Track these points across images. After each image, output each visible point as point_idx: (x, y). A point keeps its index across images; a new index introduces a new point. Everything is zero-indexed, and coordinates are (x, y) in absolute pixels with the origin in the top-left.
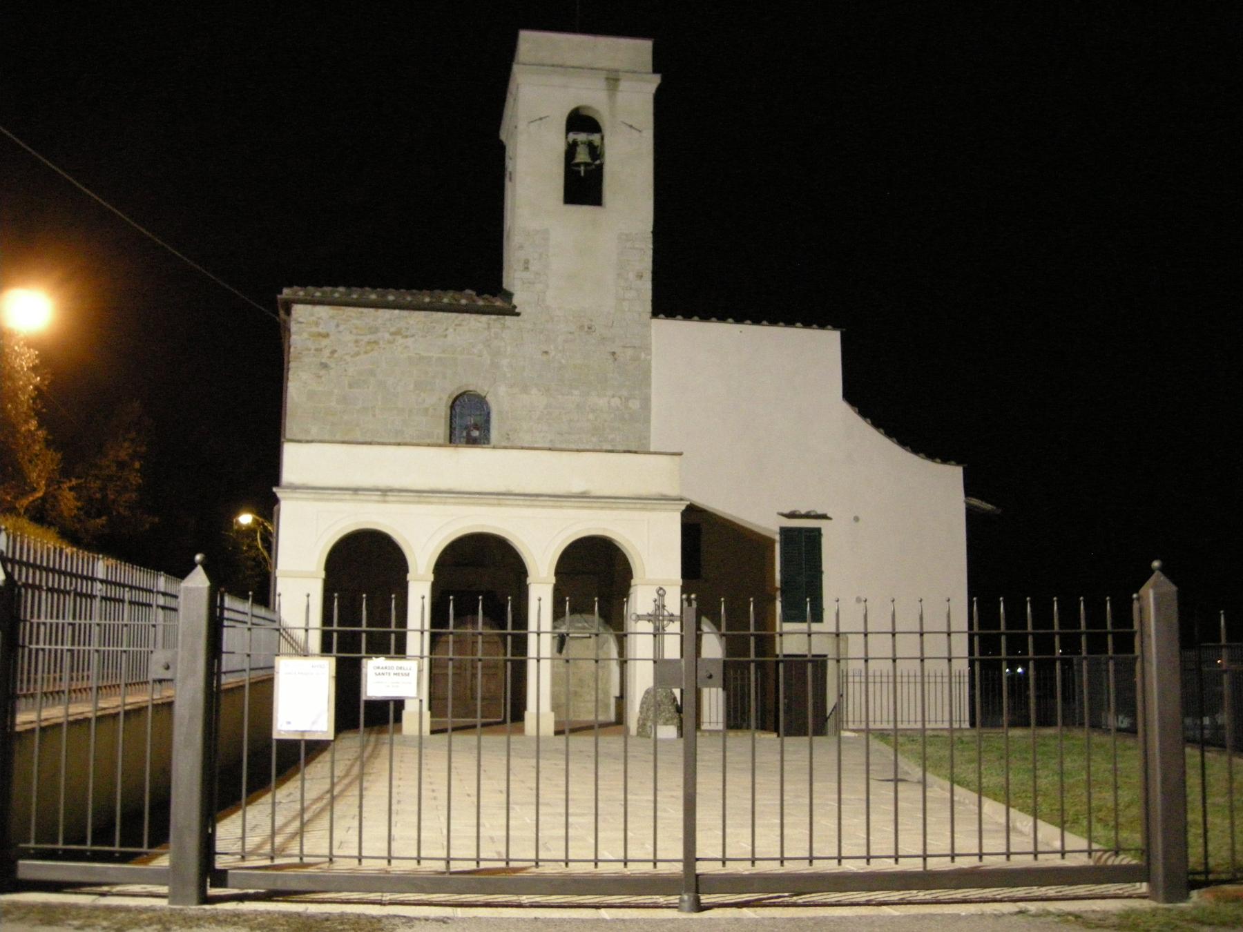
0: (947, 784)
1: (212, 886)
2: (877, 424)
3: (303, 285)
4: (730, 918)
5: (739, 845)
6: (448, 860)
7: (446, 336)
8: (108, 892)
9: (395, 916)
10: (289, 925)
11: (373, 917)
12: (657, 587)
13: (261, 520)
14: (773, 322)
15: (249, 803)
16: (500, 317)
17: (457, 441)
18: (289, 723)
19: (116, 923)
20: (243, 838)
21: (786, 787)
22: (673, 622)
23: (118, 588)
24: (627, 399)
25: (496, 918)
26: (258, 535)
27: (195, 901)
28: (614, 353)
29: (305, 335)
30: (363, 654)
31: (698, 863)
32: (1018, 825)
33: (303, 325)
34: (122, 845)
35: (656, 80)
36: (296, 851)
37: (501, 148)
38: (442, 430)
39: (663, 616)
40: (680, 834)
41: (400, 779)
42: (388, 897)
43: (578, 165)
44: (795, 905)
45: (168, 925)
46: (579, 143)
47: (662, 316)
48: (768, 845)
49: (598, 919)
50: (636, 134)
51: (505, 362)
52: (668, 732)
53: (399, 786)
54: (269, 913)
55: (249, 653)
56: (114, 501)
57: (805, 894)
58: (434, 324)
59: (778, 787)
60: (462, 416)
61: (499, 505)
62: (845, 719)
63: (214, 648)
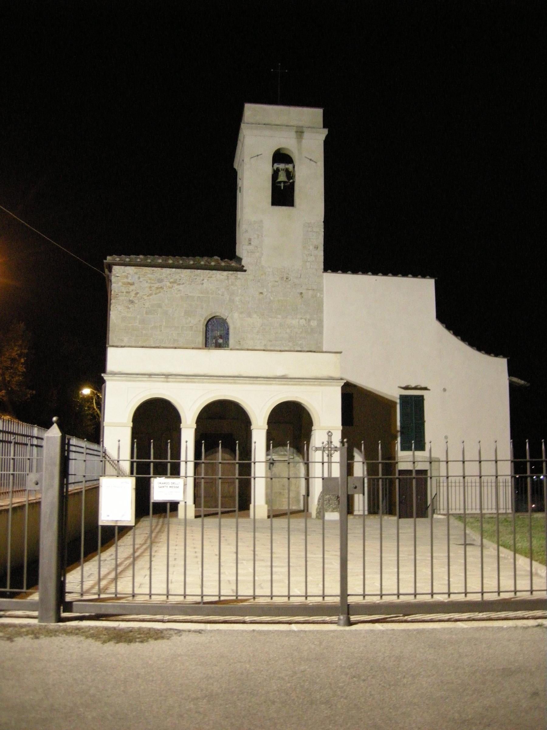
0: (495, 546)
1: (64, 612)
2: (456, 334)
3: (119, 254)
4: (368, 630)
5: (373, 587)
6: (202, 596)
7: (203, 284)
8: (3, 615)
9: (171, 629)
10: (109, 635)
11: (158, 630)
12: (327, 431)
13: (95, 392)
14: (395, 274)
15: (85, 561)
16: (235, 272)
17: (209, 346)
18: (108, 516)
19: (7, 634)
20: (82, 582)
21: (400, 549)
22: (337, 451)
23: (9, 435)
24: (309, 320)
25: (230, 630)
26: (94, 400)
27: (54, 621)
28: (301, 293)
29: (120, 284)
30: (152, 475)
31: (349, 598)
32: (539, 572)
33: (119, 278)
34: (11, 588)
35: (326, 132)
36: (113, 590)
37: (234, 174)
38: (200, 339)
39: (331, 448)
40: (338, 578)
41: (176, 545)
42: (167, 617)
43: (280, 182)
44: (406, 621)
45: (37, 635)
46: (280, 170)
47: (329, 271)
48: (390, 586)
49: (290, 631)
50: (314, 164)
51: (237, 299)
52: (333, 516)
53: (176, 550)
54: (97, 627)
55: (84, 475)
56: (9, 382)
57: (413, 614)
58: (195, 277)
59: (396, 549)
60: (212, 331)
61: (235, 383)
62: (438, 508)
63: (64, 472)
